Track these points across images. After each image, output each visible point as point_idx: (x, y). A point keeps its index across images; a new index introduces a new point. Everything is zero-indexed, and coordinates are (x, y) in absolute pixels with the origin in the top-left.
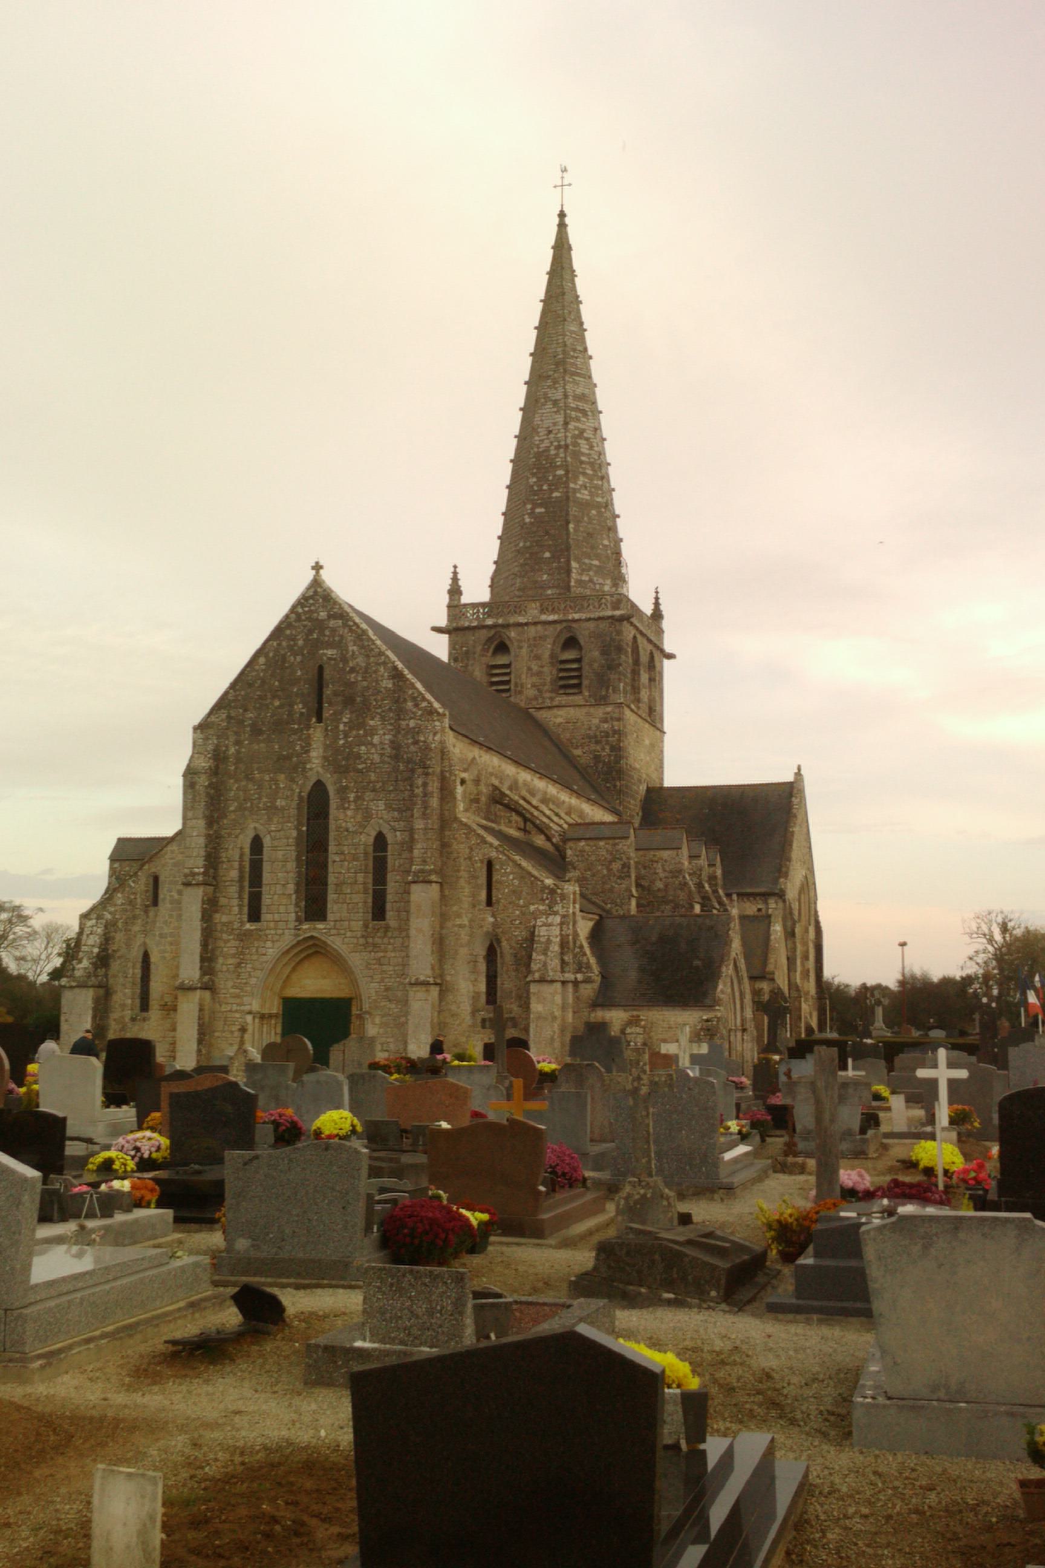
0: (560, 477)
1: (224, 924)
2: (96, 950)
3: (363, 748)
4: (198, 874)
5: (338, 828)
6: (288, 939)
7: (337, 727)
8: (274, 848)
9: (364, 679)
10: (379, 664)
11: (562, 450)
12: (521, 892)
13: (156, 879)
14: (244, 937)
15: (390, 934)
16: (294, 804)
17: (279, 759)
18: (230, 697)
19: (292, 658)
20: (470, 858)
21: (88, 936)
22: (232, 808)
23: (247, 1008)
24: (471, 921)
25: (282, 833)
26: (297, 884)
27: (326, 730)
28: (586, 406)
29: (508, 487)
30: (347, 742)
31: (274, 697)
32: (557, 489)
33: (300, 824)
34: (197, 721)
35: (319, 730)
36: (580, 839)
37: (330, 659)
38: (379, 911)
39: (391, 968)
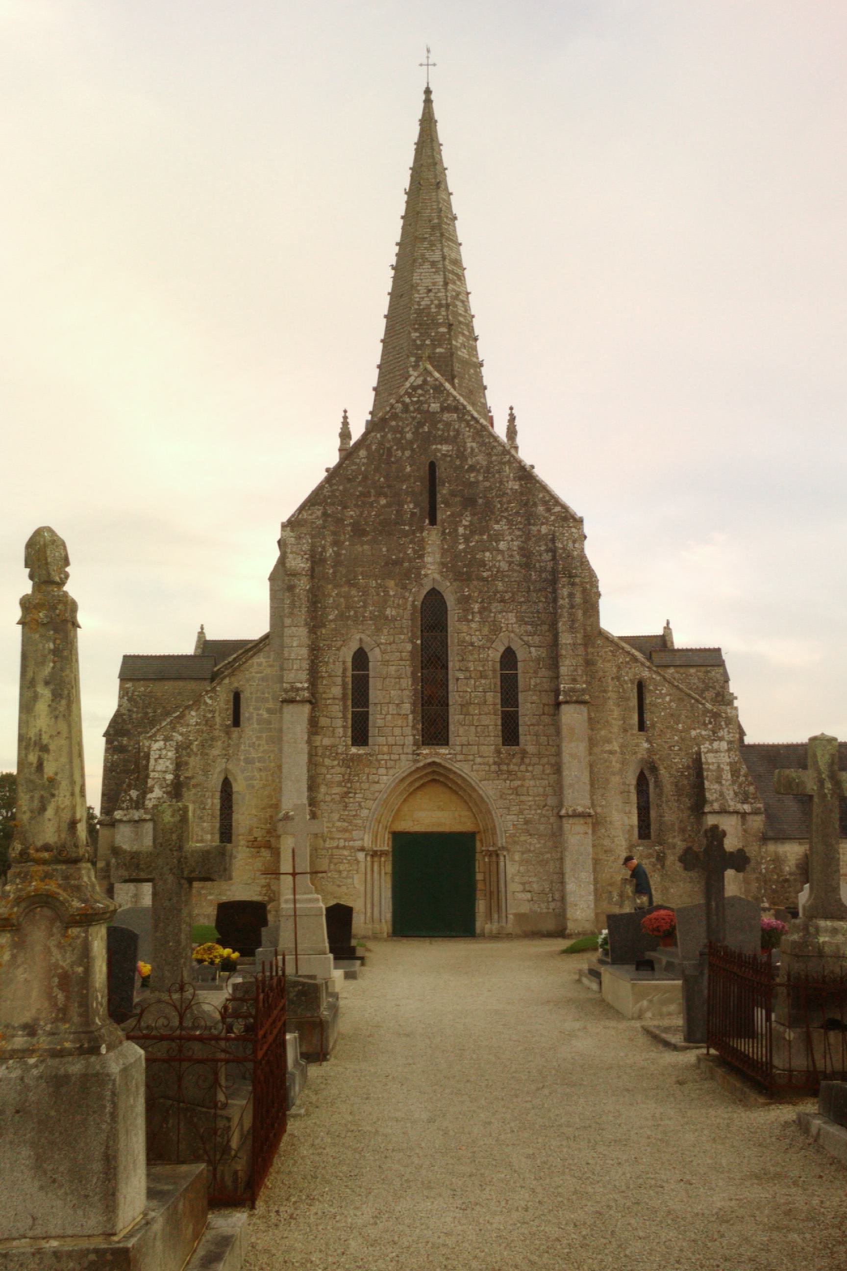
0: (443, 334)
1: (326, 748)
2: (169, 777)
3: (487, 554)
4: (303, 689)
5: (461, 642)
6: (405, 765)
7: (456, 531)
8: (386, 663)
9: (486, 479)
10: (504, 463)
11: (443, 309)
12: (680, 715)
13: (237, 697)
14: (350, 762)
15: (527, 761)
16: (407, 614)
17: (387, 564)
18: (326, 492)
19: (399, 453)
20: (618, 678)
21: (156, 760)
22: (331, 617)
23: (358, 844)
24: (622, 746)
25: (394, 646)
26: (414, 704)
27: (443, 533)
28: (452, 271)
29: (382, 341)
30: (468, 546)
31: (379, 494)
32: (440, 346)
33: (414, 636)
34: (285, 519)
35: (434, 533)
36: (668, 666)
37: (445, 455)
38: (510, 733)
39: (531, 798)
